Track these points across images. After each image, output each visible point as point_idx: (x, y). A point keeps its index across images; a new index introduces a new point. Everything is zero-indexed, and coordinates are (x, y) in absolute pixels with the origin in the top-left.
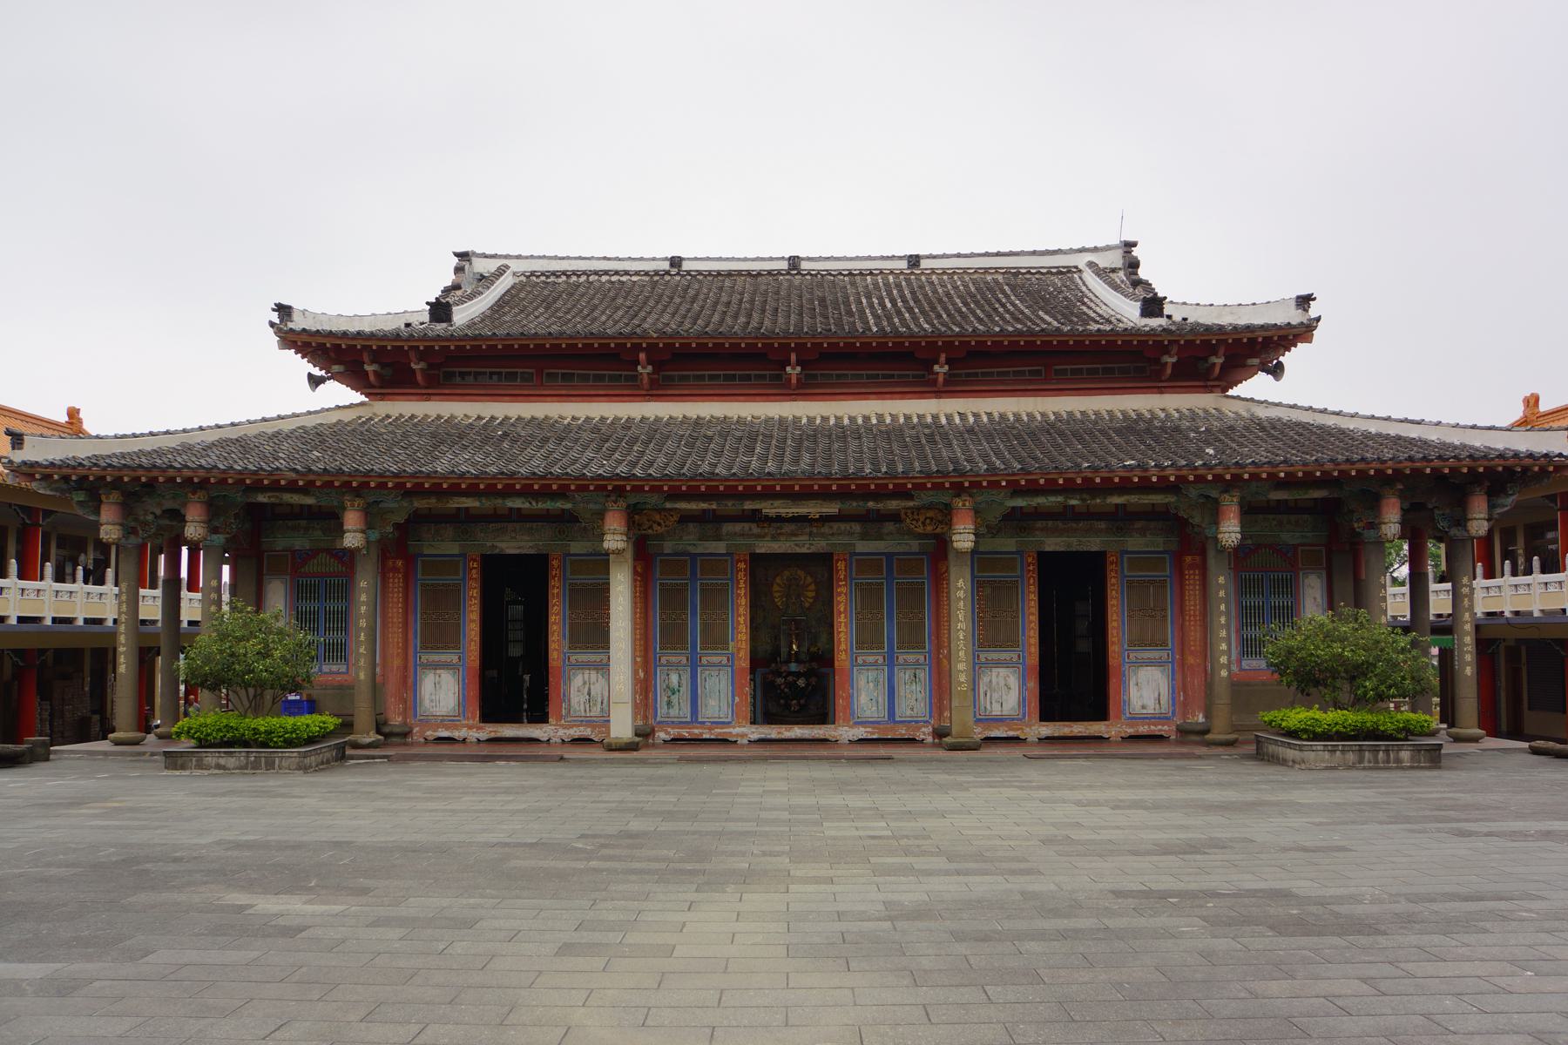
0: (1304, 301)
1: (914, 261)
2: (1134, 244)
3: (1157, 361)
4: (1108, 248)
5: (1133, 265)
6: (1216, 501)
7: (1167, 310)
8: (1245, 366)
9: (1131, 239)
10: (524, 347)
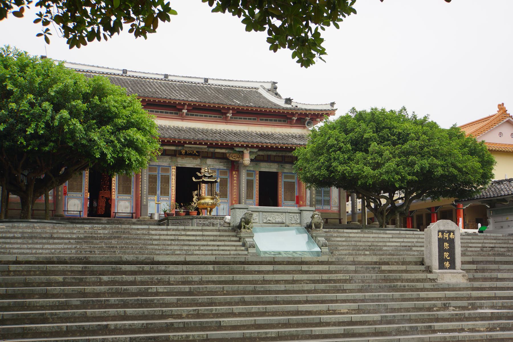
0: (332, 104)
1: (166, 76)
2: (277, 83)
3: (290, 119)
4: (268, 82)
5: (276, 88)
6: (243, 152)
7: (292, 104)
8: (316, 121)
9: (275, 81)
10: (270, 111)
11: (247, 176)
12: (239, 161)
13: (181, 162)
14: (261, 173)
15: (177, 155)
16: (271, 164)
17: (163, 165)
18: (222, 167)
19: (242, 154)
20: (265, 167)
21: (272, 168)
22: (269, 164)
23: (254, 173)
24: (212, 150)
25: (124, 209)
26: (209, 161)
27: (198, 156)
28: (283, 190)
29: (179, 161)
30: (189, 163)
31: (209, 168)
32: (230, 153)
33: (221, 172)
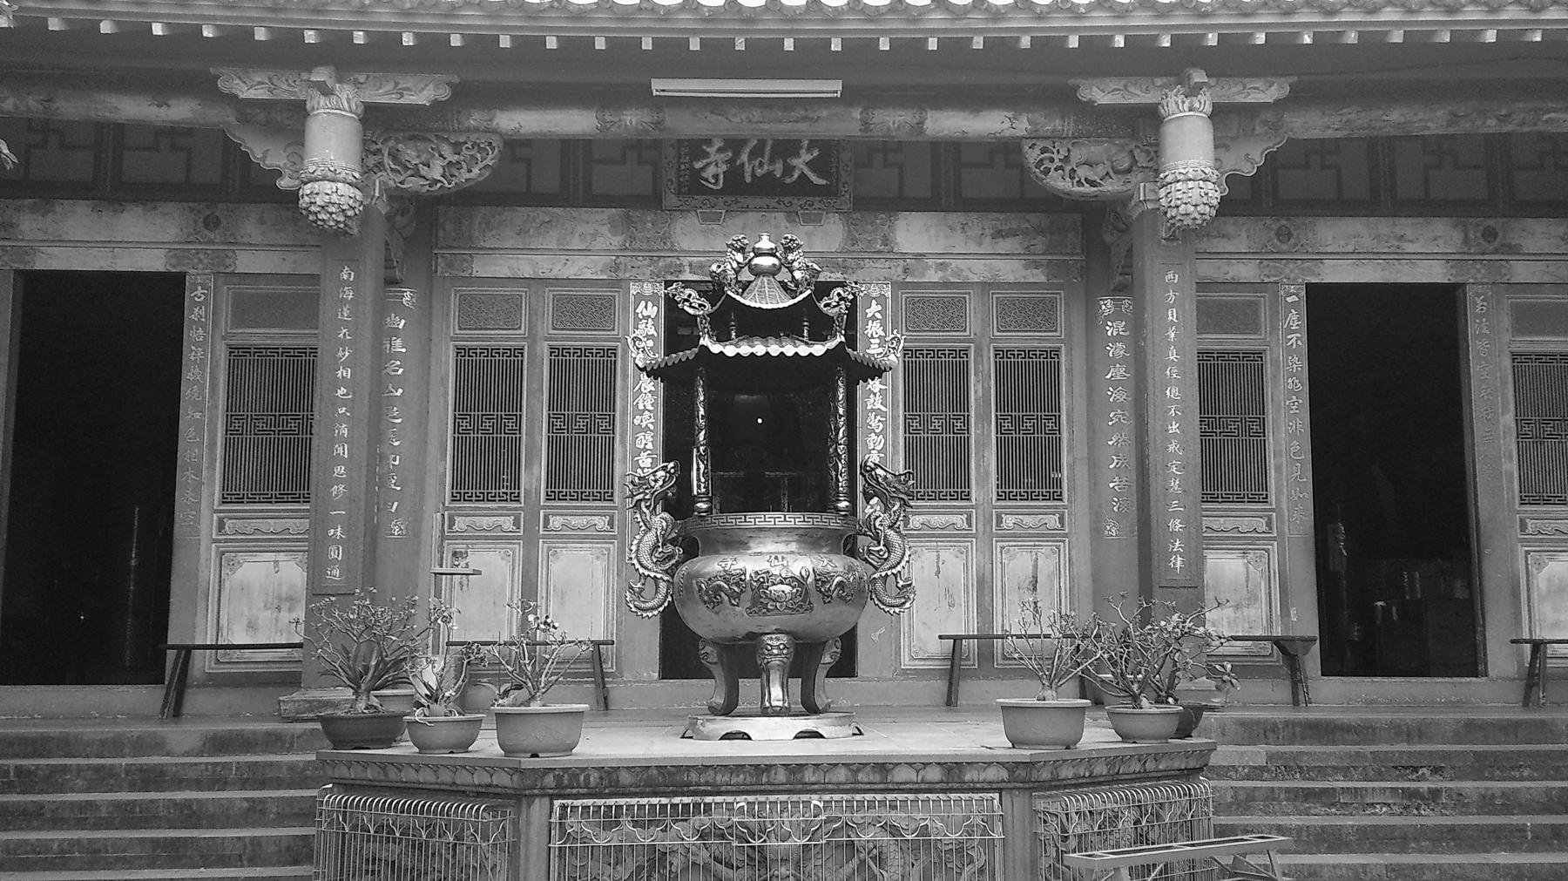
11: (1201, 329)
12: (1124, 200)
13: (699, 244)
14: (1322, 299)
15: (671, 199)
16: (1405, 226)
17: (570, 272)
18: (1010, 271)
19: (1143, 127)
20: (1355, 254)
21: (1418, 255)
22: (1384, 226)
23: (1265, 300)
24: (893, 120)
25: (265, 616)
26: (914, 234)
27: (827, 192)
28: (1509, 419)
29: (684, 243)
30: (764, 256)
31: (908, 284)
32: (1054, 137)
33: (1005, 307)
